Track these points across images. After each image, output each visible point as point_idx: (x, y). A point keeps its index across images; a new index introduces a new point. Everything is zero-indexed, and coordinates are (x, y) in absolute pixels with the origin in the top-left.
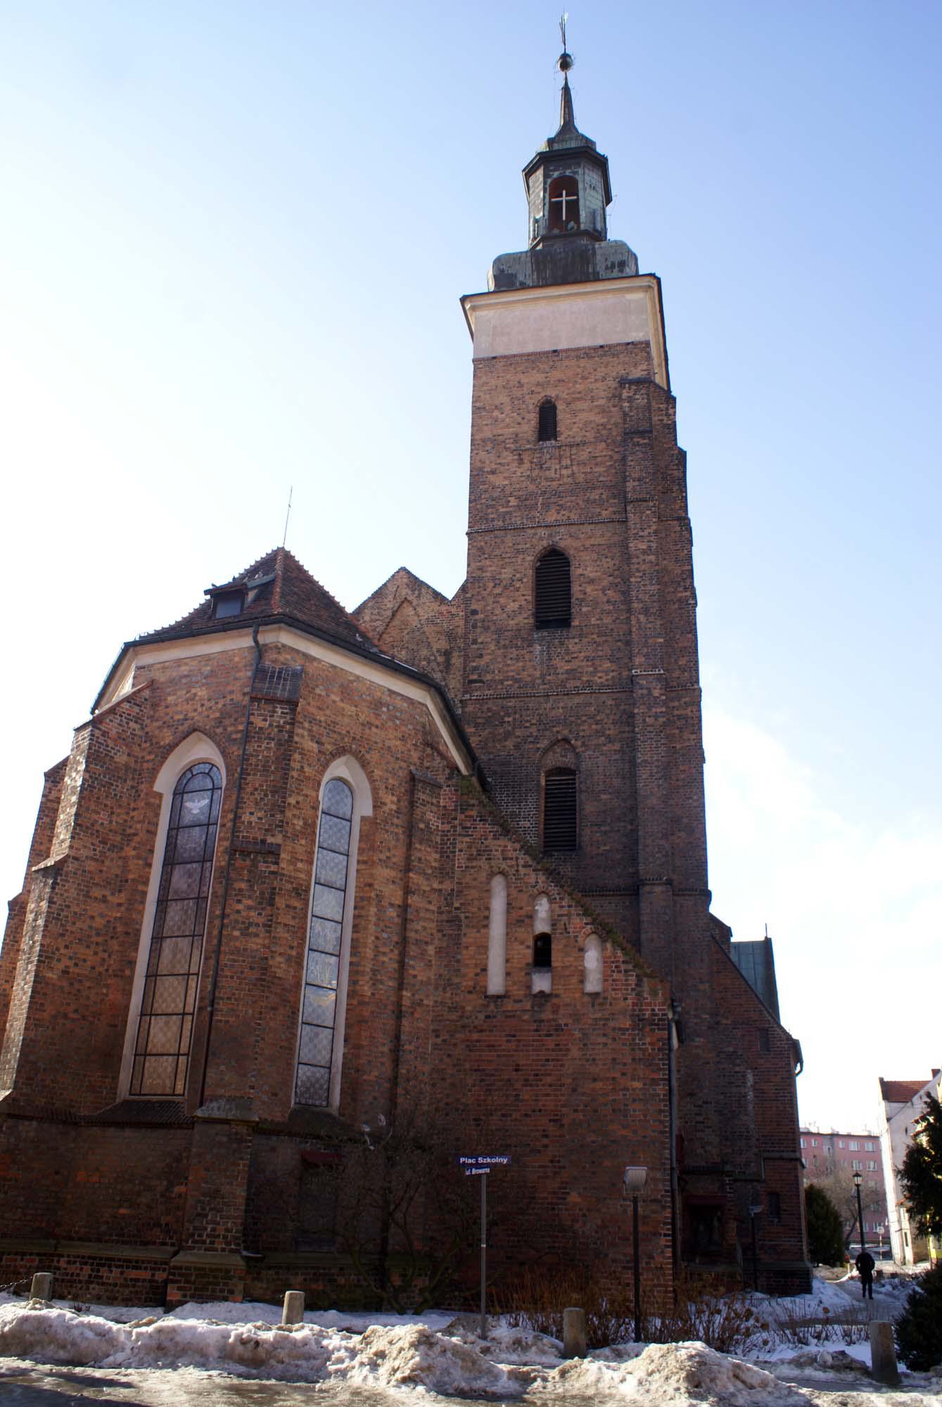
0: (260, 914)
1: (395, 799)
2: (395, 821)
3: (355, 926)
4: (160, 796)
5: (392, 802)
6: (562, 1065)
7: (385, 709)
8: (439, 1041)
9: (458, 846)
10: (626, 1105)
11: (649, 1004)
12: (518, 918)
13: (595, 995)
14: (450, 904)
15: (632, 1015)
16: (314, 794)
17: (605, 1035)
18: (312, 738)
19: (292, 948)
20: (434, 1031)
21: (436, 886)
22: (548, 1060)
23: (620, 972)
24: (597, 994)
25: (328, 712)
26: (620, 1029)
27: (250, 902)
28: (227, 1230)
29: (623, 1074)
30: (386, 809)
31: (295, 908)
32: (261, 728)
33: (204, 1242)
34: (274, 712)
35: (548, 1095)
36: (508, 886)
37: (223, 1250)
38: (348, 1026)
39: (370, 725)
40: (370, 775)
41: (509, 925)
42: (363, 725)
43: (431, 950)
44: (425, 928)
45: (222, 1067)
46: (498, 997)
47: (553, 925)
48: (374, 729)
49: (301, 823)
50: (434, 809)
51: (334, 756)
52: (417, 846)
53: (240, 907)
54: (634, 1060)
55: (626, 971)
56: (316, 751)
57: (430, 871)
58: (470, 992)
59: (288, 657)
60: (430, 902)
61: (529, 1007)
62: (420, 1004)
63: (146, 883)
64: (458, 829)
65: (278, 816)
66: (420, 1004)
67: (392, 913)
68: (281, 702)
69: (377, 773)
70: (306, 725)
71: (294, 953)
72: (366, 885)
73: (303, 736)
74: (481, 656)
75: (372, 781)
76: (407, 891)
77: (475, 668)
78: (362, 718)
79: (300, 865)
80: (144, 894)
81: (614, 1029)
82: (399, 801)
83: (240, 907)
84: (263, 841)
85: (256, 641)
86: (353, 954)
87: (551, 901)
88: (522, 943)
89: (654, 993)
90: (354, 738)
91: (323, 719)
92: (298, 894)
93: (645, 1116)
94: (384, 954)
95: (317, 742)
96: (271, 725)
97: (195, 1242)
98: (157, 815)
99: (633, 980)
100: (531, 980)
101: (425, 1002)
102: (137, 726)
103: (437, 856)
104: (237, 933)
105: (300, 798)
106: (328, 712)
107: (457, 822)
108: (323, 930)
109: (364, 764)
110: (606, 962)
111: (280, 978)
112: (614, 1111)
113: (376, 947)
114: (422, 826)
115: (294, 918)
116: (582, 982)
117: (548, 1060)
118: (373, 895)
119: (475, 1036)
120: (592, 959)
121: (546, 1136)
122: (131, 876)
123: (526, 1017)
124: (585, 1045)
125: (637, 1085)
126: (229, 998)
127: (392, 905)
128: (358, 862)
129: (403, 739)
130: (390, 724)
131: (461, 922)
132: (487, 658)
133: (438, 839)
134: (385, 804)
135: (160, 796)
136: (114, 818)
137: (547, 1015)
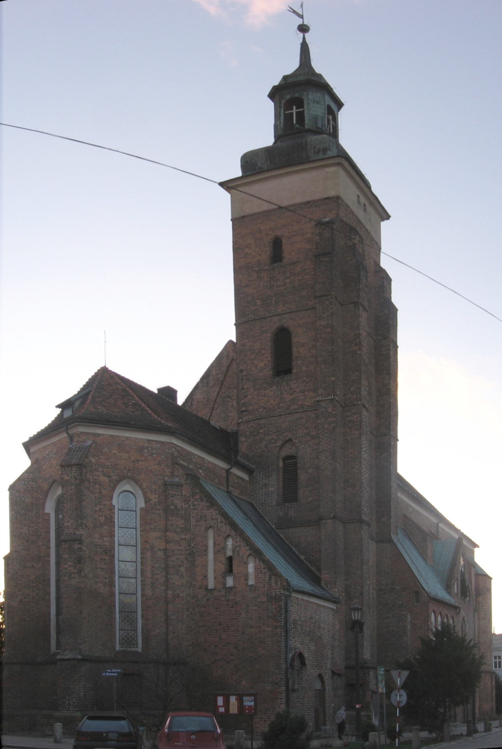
0: (75, 568)
1: (157, 496)
2: (158, 507)
3: (142, 563)
4: (49, 514)
5: (155, 498)
6: (238, 621)
7: (146, 451)
8: (188, 613)
9: (192, 515)
10: (264, 639)
11: (274, 589)
12: (220, 550)
13: (231, 588)
14: (189, 546)
15: (267, 595)
16: (109, 503)
17: (256, 605)
18: (104, 475)
19: (106, 578)
20: (186, 608)
21: (183, 537)
22: (232, 619)
23: (262, 573)
24: (252, 585)
25: (112, 460)
26: (262, 602)
27: (70, 563)
28: (74, 703)
29: (263, 624)
30: (152, 502)
31: (105, 560)
32: (67, 480)
33: (66, 708)
34: (72, 471)
35: (232, 636)
36: (214, 534)
37: (73, 710)
38: (142, 610)
39: (138, 461)
40: (141, 487)
41: (215, 553)
42: (133, 461)
43: (182, 569)
44: (178, 559)
45: (67, 637)
46: (212, 590)
47: (233, 552)
48: (140, 463)
49: (103, 518)
50: (179, 497)
51: (118, 482)
52: (170, 518)
53: (66, 566)
54: (268, 617)
55: (265, 573)
56: (107, 481)
57: (179, 530)
58: (200, 589)
59: (84, 437)
60: (180, 546)
61: (224, 594)
62: (178, 596)
63: (49, 556)
64: (191, 506)
65: (80, 521)
66: (178, 596)
67: (160, 554)
68: (74, 465)
69: (145, 485)
70: (100, 469)
71: (107, 581)
72: (145, 542)
73: (99, 475)
74: (246, 396)
75: (142, 490)
76: (167, 542)
77: (244, 404)
78: (133, 458)
79: (105, 539)
80: (49, 561)
81: (259, 602)
82: (159, 496)
83: (66, 566)
84: (74, 534)
85: (68, 434)
86: (142, 576)
87: (233, 539)
88: (220, 562)
89: (276, 583)
90: (129, 470)
91: (109, 464)
92: (106, 553)
93: (272, 644)
94: (157, 574)
95: (108, 477)
96: (71, 478)
97: (62, 708)
98: (49, 524)
99: (267, 578)
100: (225, 580)
101: (181, 595)
102: (33, 483)
103: (183, 522)
104: (66, 578)
105: (101, 507)
106: (112, 460)
107: (191, 503)
108: (126, 566)
109: (137, 482)
110: (256, 568)
111: (101, 593)
112: (260, 642)
113: (152, 571)
114: (172, 507)
115: (105, 564)
116: (247, 579)
117: (232, 619)
118: (148, 546)
119: (203, 610)
120: (251, 568)
121: (232, 655)
122: (42, 554)
123: (223, 599)
124: (247, 611)
125: (269, 629)
126: (67, 607)
127: (160, 550)
128: (141, 531)
129: (159, 464)
130: (150, 457)
131: (195, 553)
132: (249, 397)
133: (183, 512)
134: (151, 500)
135: (49, 514)
136: (31, 529)
137: (231, 598)
